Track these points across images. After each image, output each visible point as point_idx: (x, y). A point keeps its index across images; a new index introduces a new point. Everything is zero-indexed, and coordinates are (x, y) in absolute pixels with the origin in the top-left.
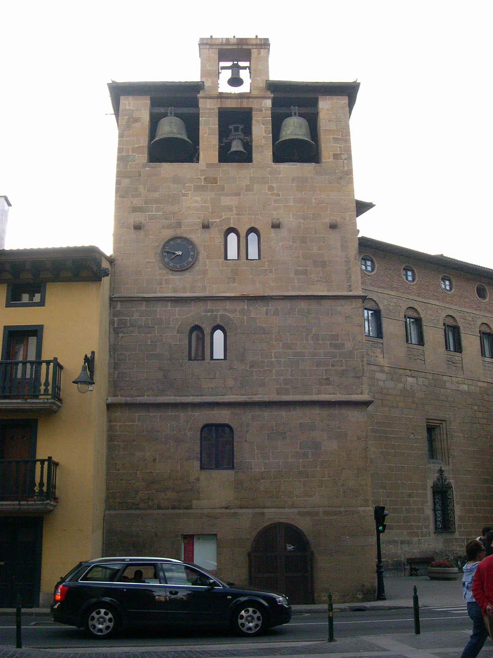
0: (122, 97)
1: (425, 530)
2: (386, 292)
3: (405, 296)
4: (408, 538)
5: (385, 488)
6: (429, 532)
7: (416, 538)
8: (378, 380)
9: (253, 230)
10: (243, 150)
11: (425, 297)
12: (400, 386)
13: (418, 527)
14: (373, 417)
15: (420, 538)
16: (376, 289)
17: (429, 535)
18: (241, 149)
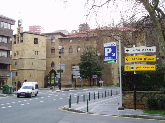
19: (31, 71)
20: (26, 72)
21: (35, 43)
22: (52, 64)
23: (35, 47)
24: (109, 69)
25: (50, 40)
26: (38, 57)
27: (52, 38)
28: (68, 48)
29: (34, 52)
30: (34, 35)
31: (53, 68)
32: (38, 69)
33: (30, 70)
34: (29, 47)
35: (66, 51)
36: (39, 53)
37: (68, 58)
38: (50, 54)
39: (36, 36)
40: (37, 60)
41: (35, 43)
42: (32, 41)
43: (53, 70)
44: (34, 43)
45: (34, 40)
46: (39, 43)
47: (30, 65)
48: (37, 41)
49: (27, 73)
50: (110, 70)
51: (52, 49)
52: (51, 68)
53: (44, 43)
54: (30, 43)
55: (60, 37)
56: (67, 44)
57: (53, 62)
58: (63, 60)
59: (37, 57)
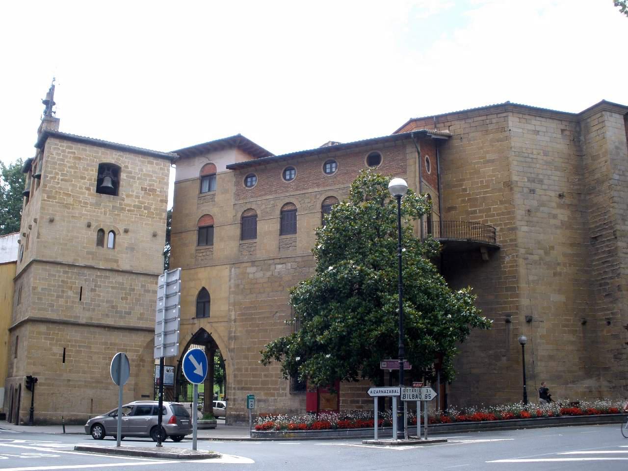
1: (281, 391)
2: (264, 198)
3: (282, 195)
4: (263, 398)
5: (248, 358)
6: (286, 393)
7: (273, 398)
8: (248, 274)
9: (112, 231)
10: (112, 186)
11: (304, 189)
12: (269, 274)
13: (275, 389)
14: (241, 304)
15: (276, 398)
17: (286, 395)
18: (110, 185)
19: (72, 334)
20: (39, 333)
21: (101, 190)
22: (198, 303)
23: (103, 210)
24: (508, 322)
25: (193, 180)
26: (116, 261)
27: (202, 171)
28: (278, 212)
29: (94, 236)
30: (101, 150)
31: (202, 320)
32: (110, 322)
33: (128, 369)
34: (67, 206)
35: (268, 228)
36: (122, 238)
37: (272, 267)
38: (193, 251)
39: (111, 158)
40: (108, 274)
41: (101, 190)
42: (83, 178)
43: (202, 331)
44: (94, 189)
45: (94, 174)
46: (123, 190)
47: (62, 301)
48: (116, 183)
49: (46, 339)
50: (511, 327)
51: (203, 224)
52: (196, 321)
53: (154, 190)
54: (73, 185)
55: (235, 157)
56: (271, 192)
57: (204, 289)
58: (251, 276)
59: (107, 260)
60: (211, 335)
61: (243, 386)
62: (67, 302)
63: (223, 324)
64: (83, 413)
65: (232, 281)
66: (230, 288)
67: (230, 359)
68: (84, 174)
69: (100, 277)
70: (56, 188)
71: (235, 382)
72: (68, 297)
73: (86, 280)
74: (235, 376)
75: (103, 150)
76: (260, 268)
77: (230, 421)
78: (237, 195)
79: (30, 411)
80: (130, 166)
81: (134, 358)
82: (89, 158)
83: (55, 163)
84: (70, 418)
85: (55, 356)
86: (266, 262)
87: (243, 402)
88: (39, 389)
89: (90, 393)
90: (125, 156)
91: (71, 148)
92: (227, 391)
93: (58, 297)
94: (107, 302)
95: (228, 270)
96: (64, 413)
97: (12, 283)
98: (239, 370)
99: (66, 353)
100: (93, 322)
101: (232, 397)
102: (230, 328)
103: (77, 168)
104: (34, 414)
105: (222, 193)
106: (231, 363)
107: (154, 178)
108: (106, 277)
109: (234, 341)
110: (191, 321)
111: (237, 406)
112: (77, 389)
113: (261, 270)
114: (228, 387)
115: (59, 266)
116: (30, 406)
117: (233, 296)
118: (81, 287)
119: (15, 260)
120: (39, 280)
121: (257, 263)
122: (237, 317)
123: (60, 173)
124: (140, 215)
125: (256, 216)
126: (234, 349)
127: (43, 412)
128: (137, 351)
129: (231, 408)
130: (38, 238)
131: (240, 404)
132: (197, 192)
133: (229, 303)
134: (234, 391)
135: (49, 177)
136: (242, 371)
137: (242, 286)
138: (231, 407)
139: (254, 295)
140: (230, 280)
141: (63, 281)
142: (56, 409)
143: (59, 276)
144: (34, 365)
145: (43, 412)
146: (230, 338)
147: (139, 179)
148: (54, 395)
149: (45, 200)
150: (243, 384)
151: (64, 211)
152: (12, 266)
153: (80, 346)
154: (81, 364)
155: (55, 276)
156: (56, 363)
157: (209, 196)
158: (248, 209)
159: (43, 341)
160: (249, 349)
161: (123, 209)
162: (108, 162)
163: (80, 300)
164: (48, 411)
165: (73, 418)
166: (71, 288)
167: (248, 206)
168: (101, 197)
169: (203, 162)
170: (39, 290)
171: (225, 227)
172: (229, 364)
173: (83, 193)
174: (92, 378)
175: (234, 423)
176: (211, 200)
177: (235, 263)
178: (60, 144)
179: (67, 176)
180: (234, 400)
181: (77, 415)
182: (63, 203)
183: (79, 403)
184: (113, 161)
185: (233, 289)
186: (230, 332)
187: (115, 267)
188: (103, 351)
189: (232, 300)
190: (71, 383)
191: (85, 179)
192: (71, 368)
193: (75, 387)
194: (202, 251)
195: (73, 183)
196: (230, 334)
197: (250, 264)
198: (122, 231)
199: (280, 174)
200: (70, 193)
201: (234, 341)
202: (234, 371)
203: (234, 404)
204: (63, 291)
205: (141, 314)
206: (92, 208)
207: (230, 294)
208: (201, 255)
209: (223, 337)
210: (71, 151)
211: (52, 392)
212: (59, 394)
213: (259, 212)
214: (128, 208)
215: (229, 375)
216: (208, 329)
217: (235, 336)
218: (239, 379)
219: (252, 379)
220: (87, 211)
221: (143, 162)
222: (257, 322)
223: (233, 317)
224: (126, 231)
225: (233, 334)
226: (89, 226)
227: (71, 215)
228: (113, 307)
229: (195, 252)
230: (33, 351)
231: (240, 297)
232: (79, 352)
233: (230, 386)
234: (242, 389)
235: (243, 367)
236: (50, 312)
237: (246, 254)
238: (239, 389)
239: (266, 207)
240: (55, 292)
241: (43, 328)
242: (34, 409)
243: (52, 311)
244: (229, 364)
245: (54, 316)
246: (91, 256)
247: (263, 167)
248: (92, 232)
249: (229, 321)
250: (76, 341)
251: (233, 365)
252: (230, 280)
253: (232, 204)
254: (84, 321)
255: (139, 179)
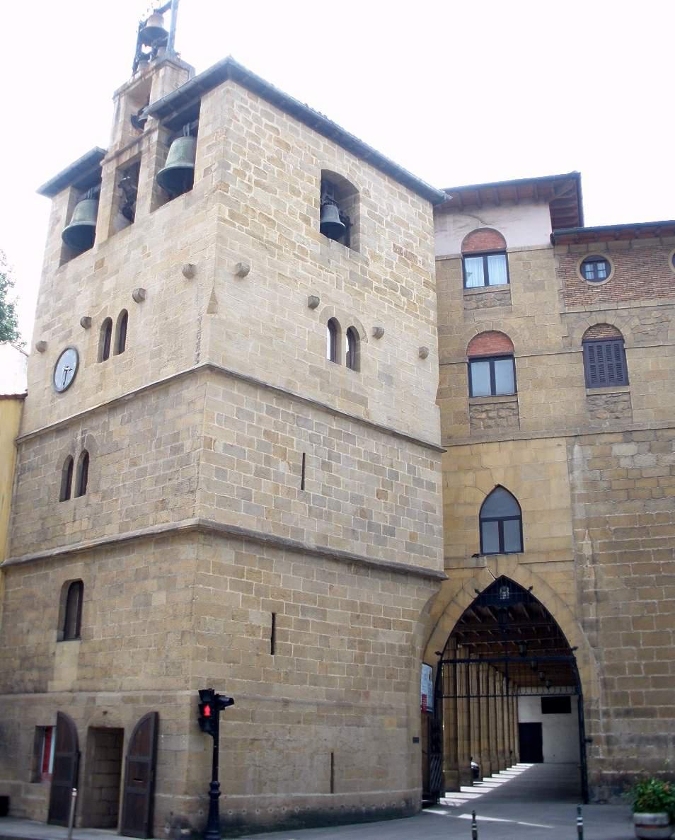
0: (466, 259)
5: (636, 643)
8: (617, 458)
16: (614, 306)
20: (220, 569)
26: (363, 401)
27: (464, 245)
32: (357, 549)
39: (343, 165)
40: (351, 429)
47: (266, 485)
49: (235, 585)
58: (625, 463)
59: (348, 395)
60: (532, 592)
61: (631, 705)
62: (276, 490)
63: (561, 566)
64: (315, 792)
65: (576, 473)
66: (573, 488)
67: (588, 645)
68: (297, 184)
69: (337, 434)
70: (245, 198)
71: (607, 697)
72: (279, 477)
73: (311, 438)
74: (606, 684)
75: (327, 144)
76: (645, 447)
77: (602, 793)
78: (566, 295)
79: (210, 794)
80: (372, 193)
81: (402, 643)
82: (303, 152)
83: (243, 141)
84: (290, 808)
85: (253, 634)
86: (659, 433)
87: (634, 746)
88: (227, 722)
89: (327, 734)
90: (362, 168)
91: (271, 119)
92: (586, 720)
93: (261, 473)
94: (355, 499)
95: (563, 448)
96: (278, 795)
97: (12, 448)
98: (614, 669)
99: (277, 628)
100: (329, 547)
101: (603, 735)
102: (583, 575)
103: (283, 165)
104: (221, 805)
105: (527, 289)
106: (592, 657)
107: (412, 232)
108: (349, 438)
109: (594, 604)
110: (473, 562)
111: (618, 756)
112: (302, 725)
113: (650, 451)
114: (589, 712)
115: (259, 392)
116: (210, 781)
117: (582, 504)
118: (304, 454)
119: (21, 392)
120: (219, 422)
121: (636, 436)
122: (597, 552)
123: (253, 166)
124: (395, 304)
125: (622, 339)
126: (597, 621)
127: (234, 796)
128: (407, 627)
129: (602, 761)
130: (211, 310)
131: (627, 750)
132: (462, 287)
133: (573, 521)
134: (605, 720)
135: (232, 169)
136: (624, 673)
137: (604, 485)
138: (601, 757)
139: (638, 504)
140: (571, 472)
141: (267, 433)
142: (260, 785)
143: (260, 420)
144: (211, 658)
145: (234, 796)
146: (583, 598)
147: (388, 225)
148: (256, 743)
149: (225, 221)
150: (630, 703)
151: (264, 258)
152: (12, 405)
153: (304, 610)
154: (308, 659)
155: (249, 416)
156: (258, 655)
157: (493, 295)
158: (598, 325)
159: (228, 590)
160: (637, 622)
161: (366, 284)
162: (336, 171)
163: (302, 488)
164: (244, 793)
165: (297, 809)
166: (284, 455)
167: (600, 319)
168: (329, 245)
169: (467, 225)
170: (219, 448)
171: (545, 359)
172: (585, 656)
173: (298, 228)
174: (329, 697)
175: (614, 798)
176: (498, 303)
177: (579, 434)
178: (250, 101)
179: (266, 179)
180: (609, 741)
181: (304, 800)
182: (261, 239)
183: (308, 764)
184: (345, 173)
185: (580, 491)
186: (582, 585)
187: (363, 416)
188: (349, 625)
189: (580, 515)
190: (292, 710)
191: (299, 196)
192: (289, 668)
193: (299, 722)
194: (486, 407)
195: (277, 196)
196: (582, 588)
197: (620, 437)
198: (369, 334)
199: (664, 259)
200: (272, 217)
201: (594, 604)
202: (602, 671)
203: (610, 752)
204: (268, 460)
205: (413, 536)
206: (315, 265)
207: (573, 501)
208: (484, 415)
209: (563, 597)
210: (270, 123)
211: (252, 737)
212: (267, 740)
213: (626, 332)
214: (375, 284)
215: (589, 683)
216: (521, 578)
217: (596, 593)
218: (617, 690)
219: (652, 689)
220: (305, 270)
221: (392, 192)
222: (653, 561)
223: (587, 552)
224: (378, 334)
225: (592, 590)
226: (313, 305)
227: (278, 271)
228: (363, 513)
229: (467, 410)
230: (207, 618)
231: (602, 508)
232: (303, 624)
233: (593, 708)
234: (628, 713)
235: (627, 663)
236: (242, 513)
237: (605, 415)
238: (618, 714)
239: (643, 322)
240: (254, 460)
241: (226, 554)
242: (220, 789)
243: (248, 509)
244: (585, 656)
245: (251, 524)
246: (318, 380)
247: (625, 243)
248: (318, 322)
249: (580, 559)
250: (297, 596)
251: (598, 658)
252: (571, 472)
253: (557, 312)
254: (311, 543)
255: (388, 225)
